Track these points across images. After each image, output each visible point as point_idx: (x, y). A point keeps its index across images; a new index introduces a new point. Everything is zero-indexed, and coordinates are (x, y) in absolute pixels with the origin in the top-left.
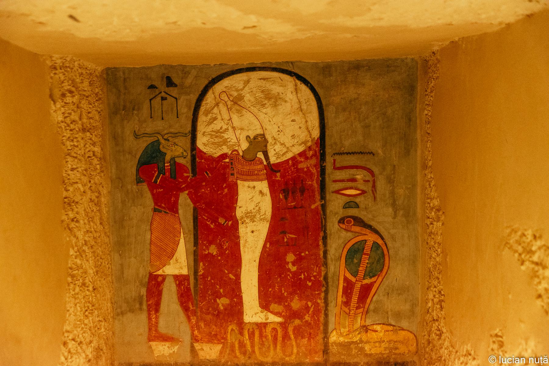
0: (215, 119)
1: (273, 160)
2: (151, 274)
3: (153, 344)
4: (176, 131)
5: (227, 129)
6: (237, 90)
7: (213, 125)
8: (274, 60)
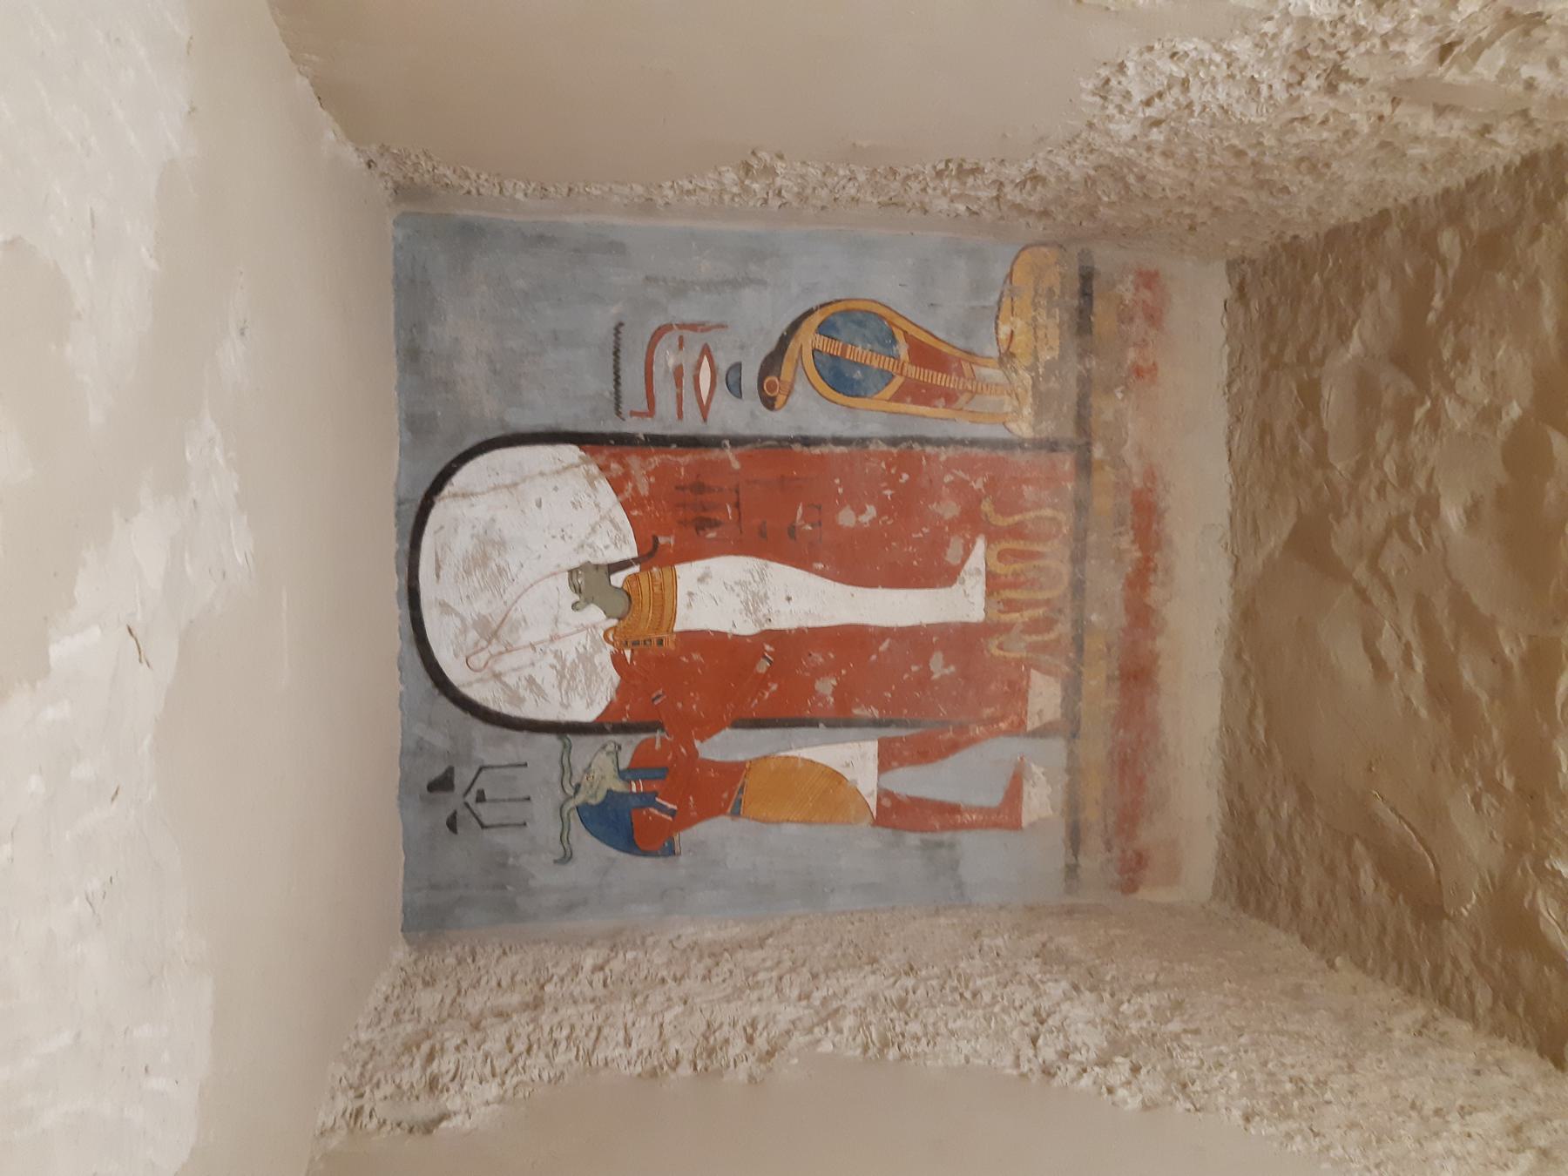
0: (531, 681)
1: (630, 551)
2: (877, 822)
3: (1026, 819)
4: (559, 768)
5: (556, 654)
6: (465, 631)
7: (547, 687)
8: (390, 544)
